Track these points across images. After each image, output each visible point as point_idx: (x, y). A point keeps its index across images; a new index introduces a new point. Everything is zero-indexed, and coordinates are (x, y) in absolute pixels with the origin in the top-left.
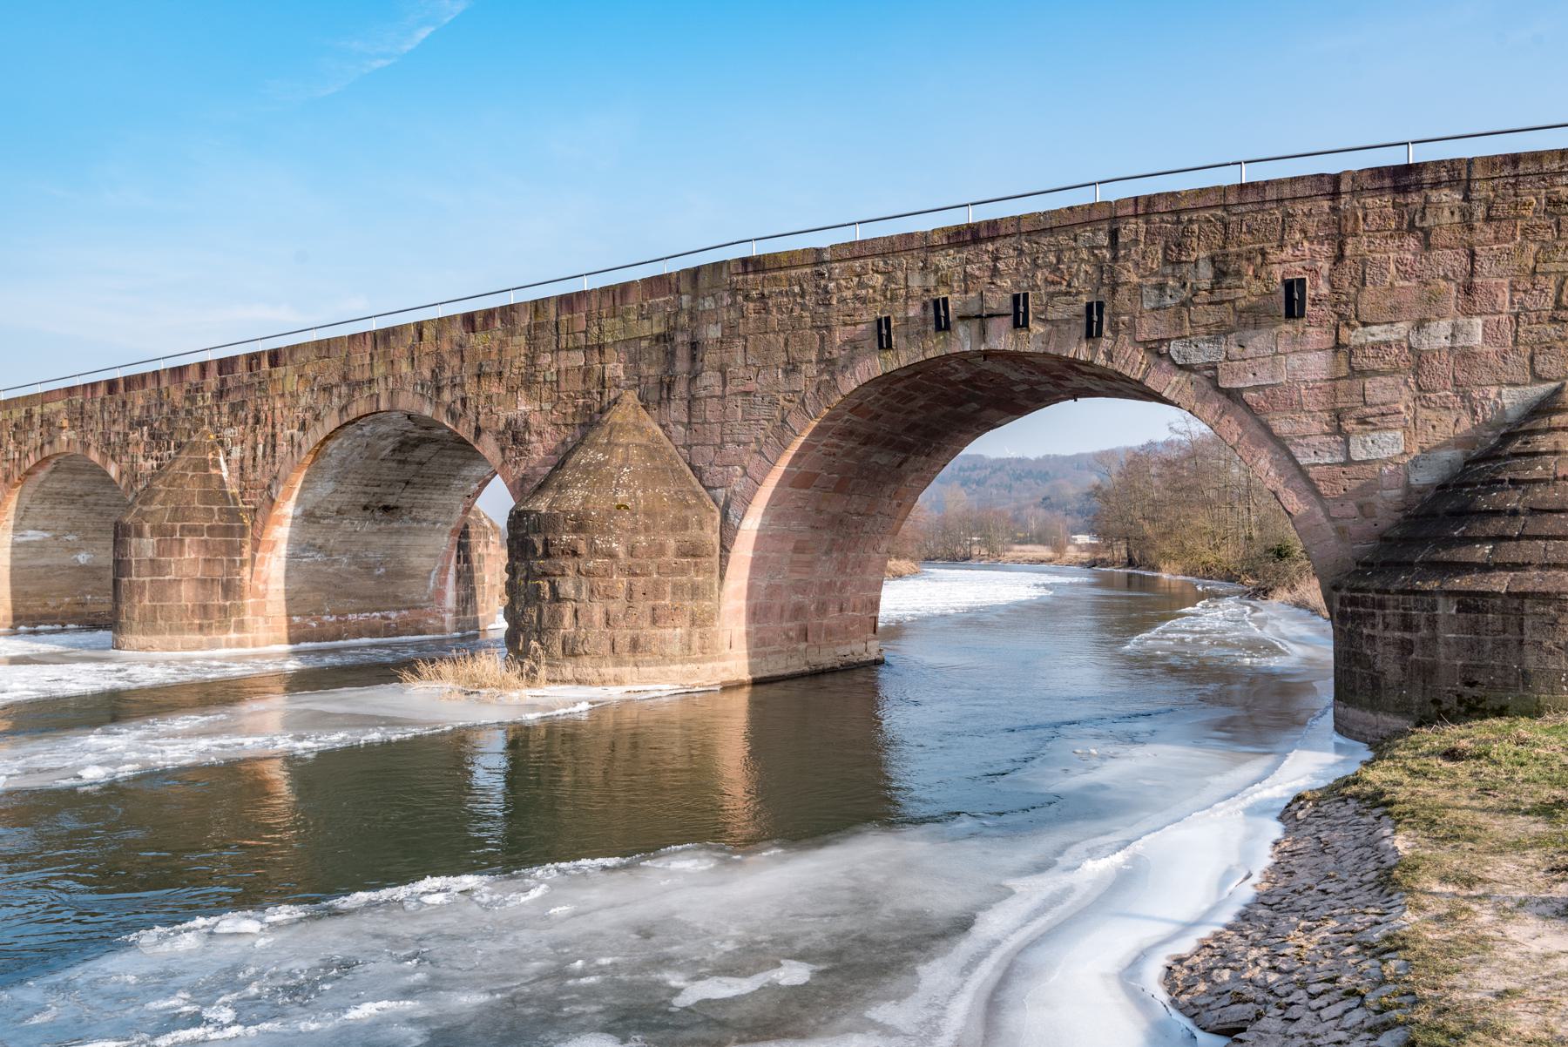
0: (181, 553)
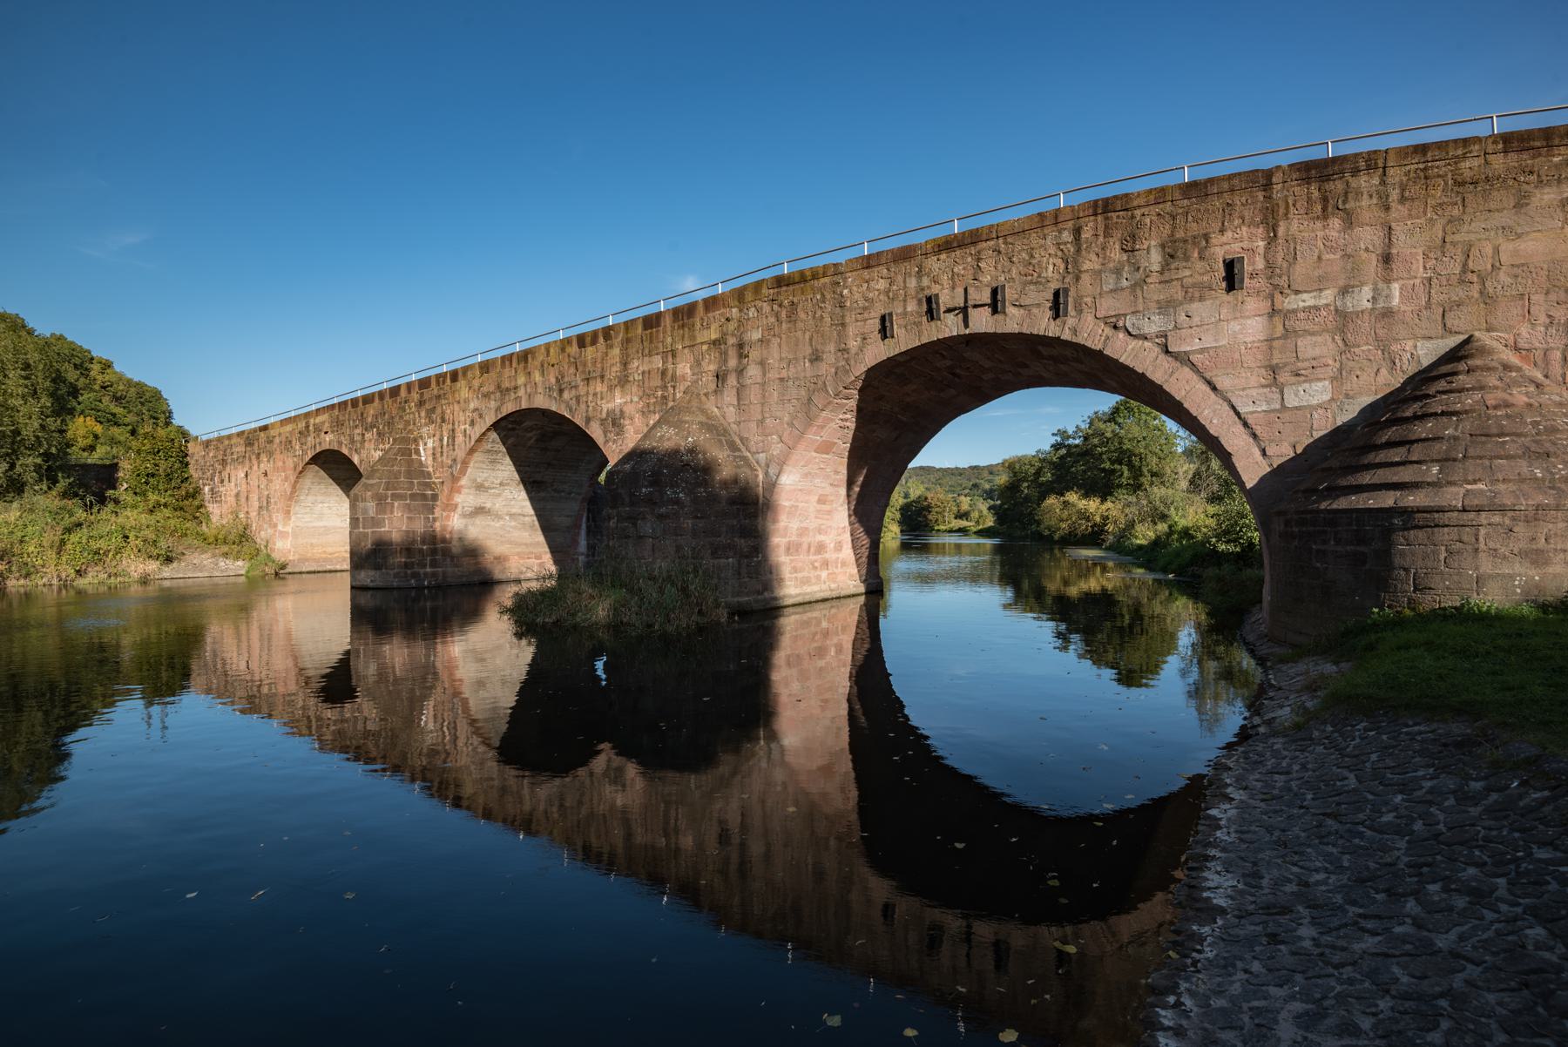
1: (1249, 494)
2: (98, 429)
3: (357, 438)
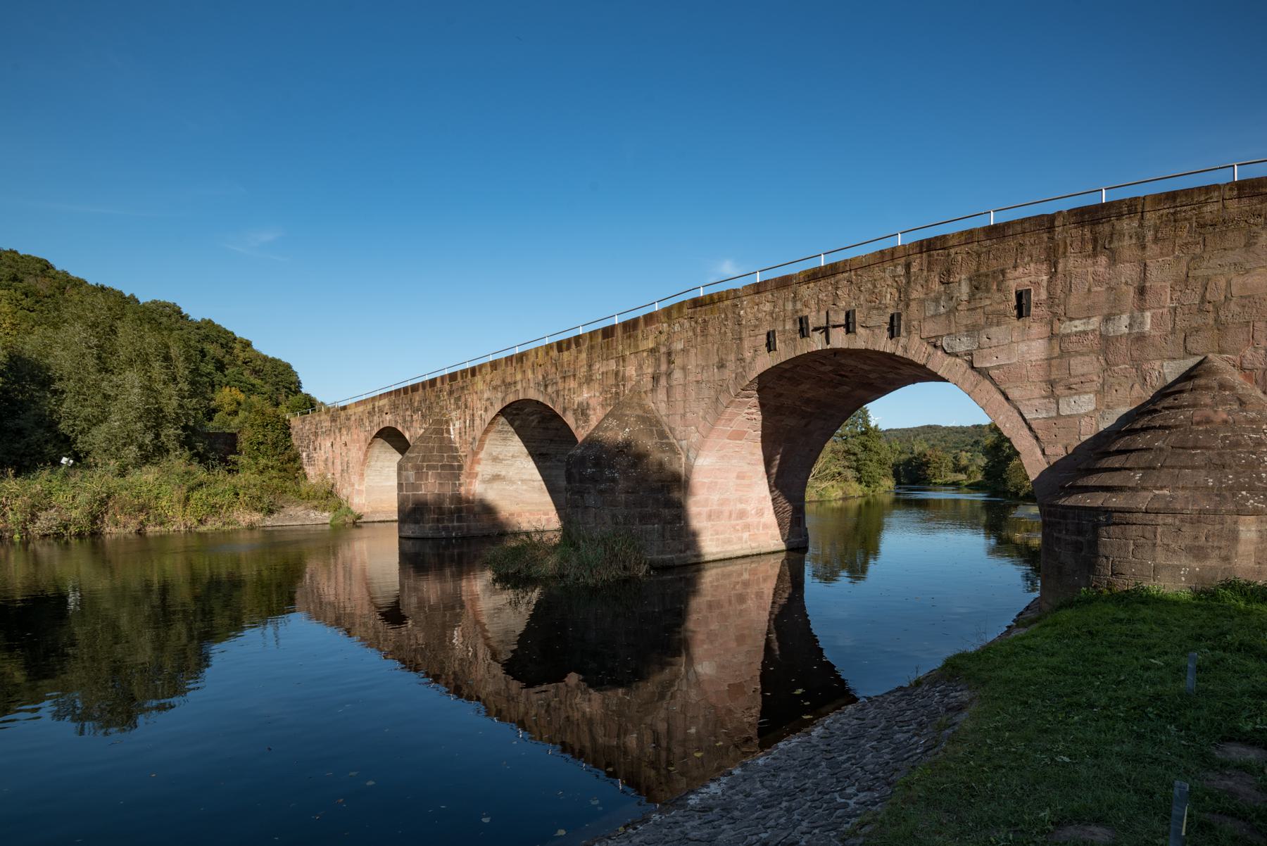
2: (241, 397)
3: (408, 418)
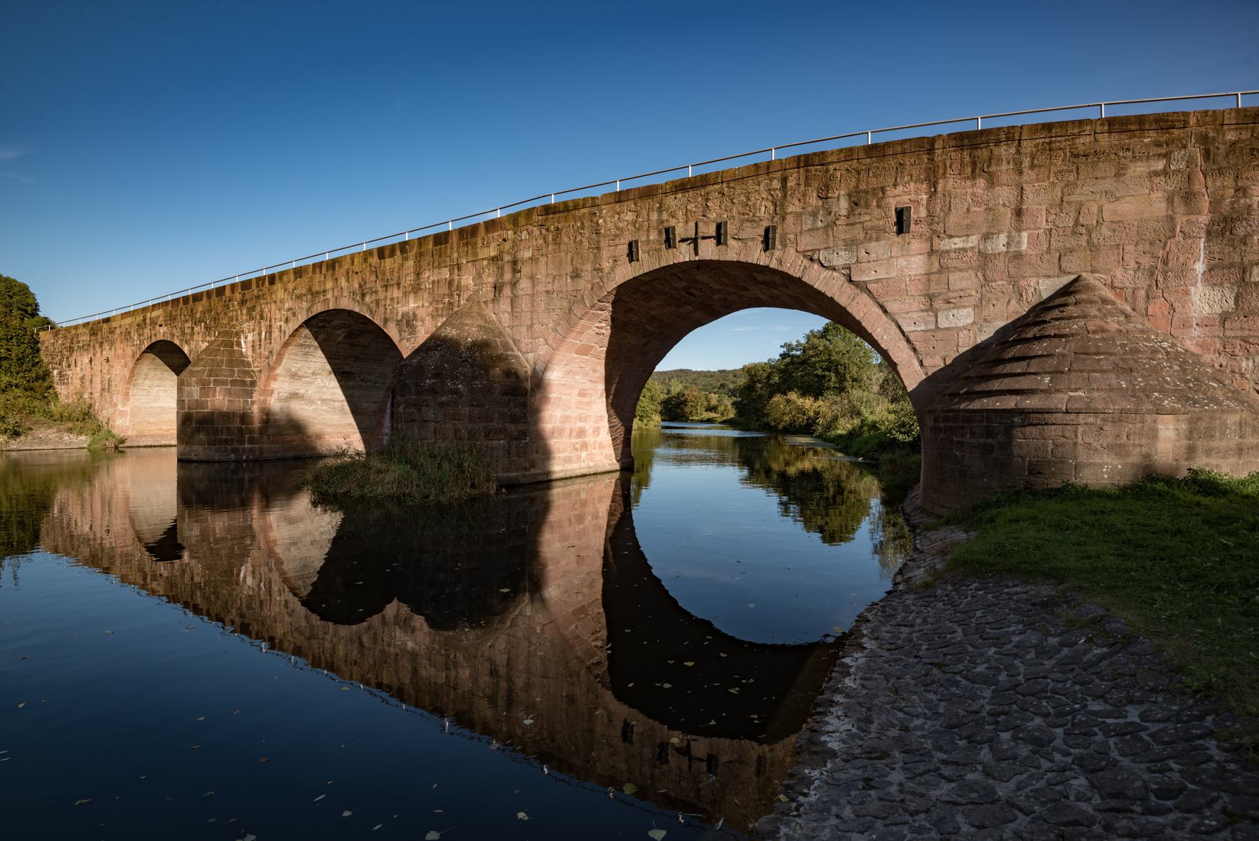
0: (214, 396)
1: (911, 394)
